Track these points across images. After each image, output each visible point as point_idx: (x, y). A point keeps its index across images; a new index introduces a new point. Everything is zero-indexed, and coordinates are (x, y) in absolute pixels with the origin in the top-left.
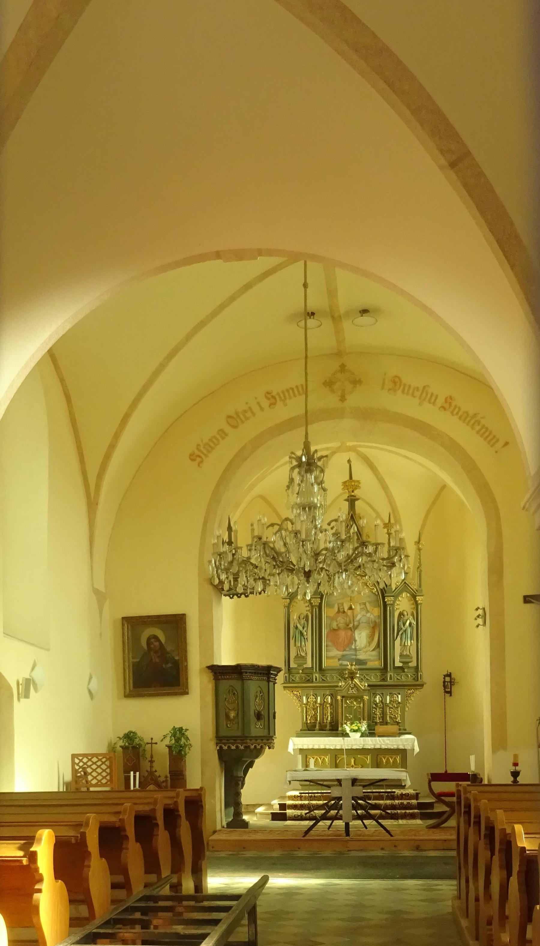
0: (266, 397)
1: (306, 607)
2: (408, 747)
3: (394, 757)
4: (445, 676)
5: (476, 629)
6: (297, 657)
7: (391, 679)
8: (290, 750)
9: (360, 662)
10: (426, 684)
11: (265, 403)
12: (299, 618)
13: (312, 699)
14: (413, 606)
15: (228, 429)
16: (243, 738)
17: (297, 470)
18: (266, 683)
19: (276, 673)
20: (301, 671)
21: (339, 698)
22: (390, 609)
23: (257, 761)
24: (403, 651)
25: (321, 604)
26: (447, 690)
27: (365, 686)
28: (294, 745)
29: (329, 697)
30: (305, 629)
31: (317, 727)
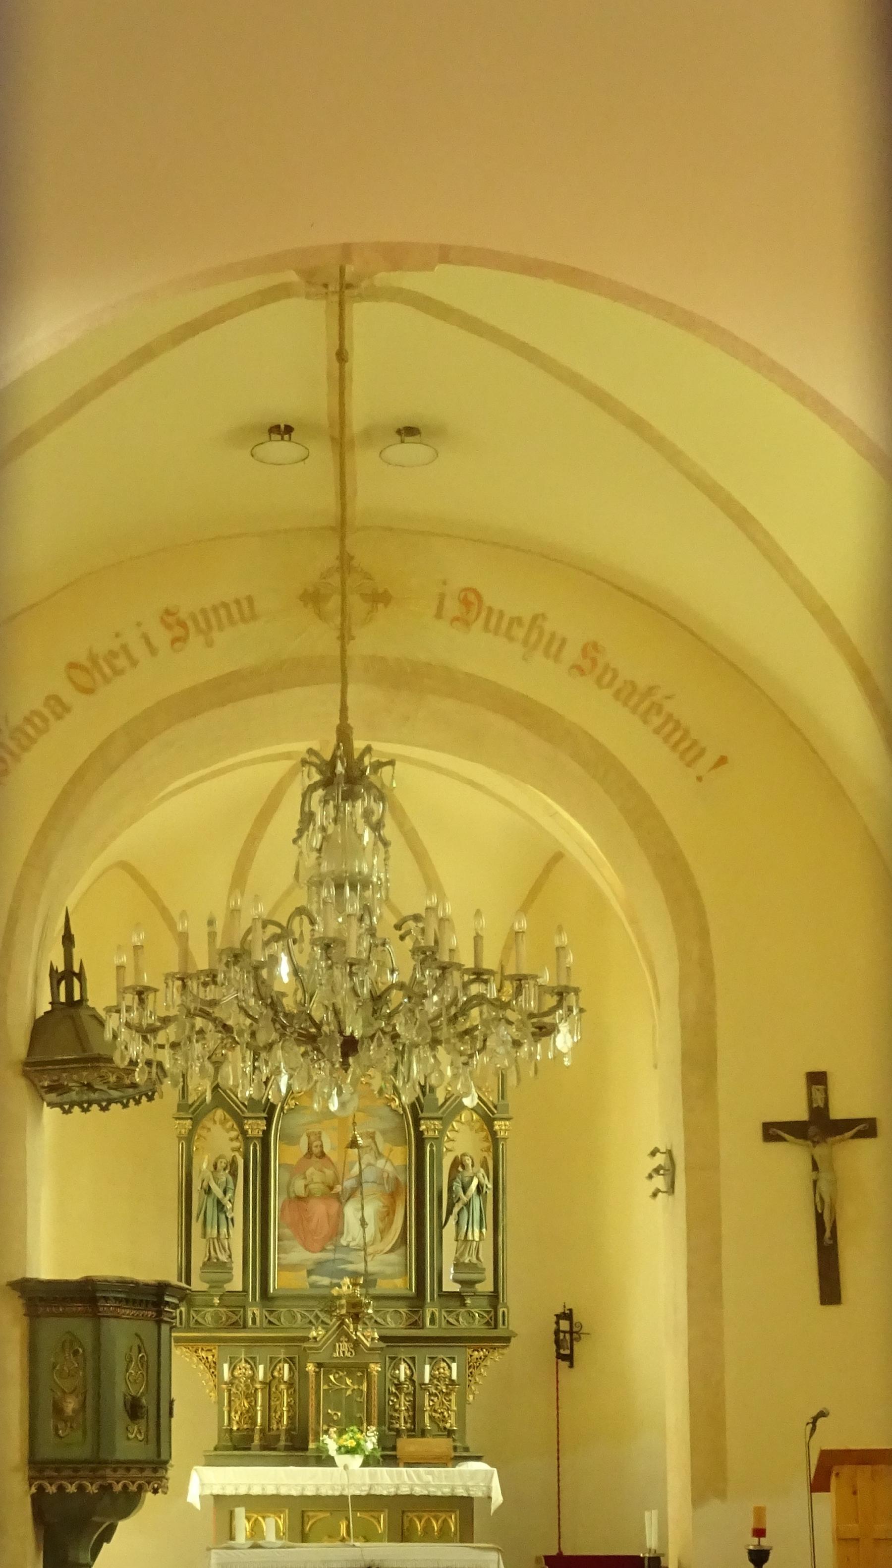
0: (163, 621)
1: (232, 1140)
2: (477, 1493)
3: (443, 1516)
4: (559, 1317)
5: (651, 1201)
6: (210, 1264)
7: (432, 1321)
8: (194, 1497)
9: (369, 1280)
10: (515, 1335)
11: (161, 637)
12: (215, 1167)
13: (243, 1370)
14: (486, 1144)
15: (68, 694)
16: (96, 1465)
17: (320, 792)
18: (151, 1326)
19: (175, 1301)
20: (217, 1301)
21: (311, 1368)
22: (431, 1151)
23: (122, 1525)
24: (462, 1255)
25: (267, 1133)
26: (562, 1352)
27: (373, 1339)
28: (203, 1485)
29: (286, 1366)
30: (229, 1195)
31: (256, 1441)
